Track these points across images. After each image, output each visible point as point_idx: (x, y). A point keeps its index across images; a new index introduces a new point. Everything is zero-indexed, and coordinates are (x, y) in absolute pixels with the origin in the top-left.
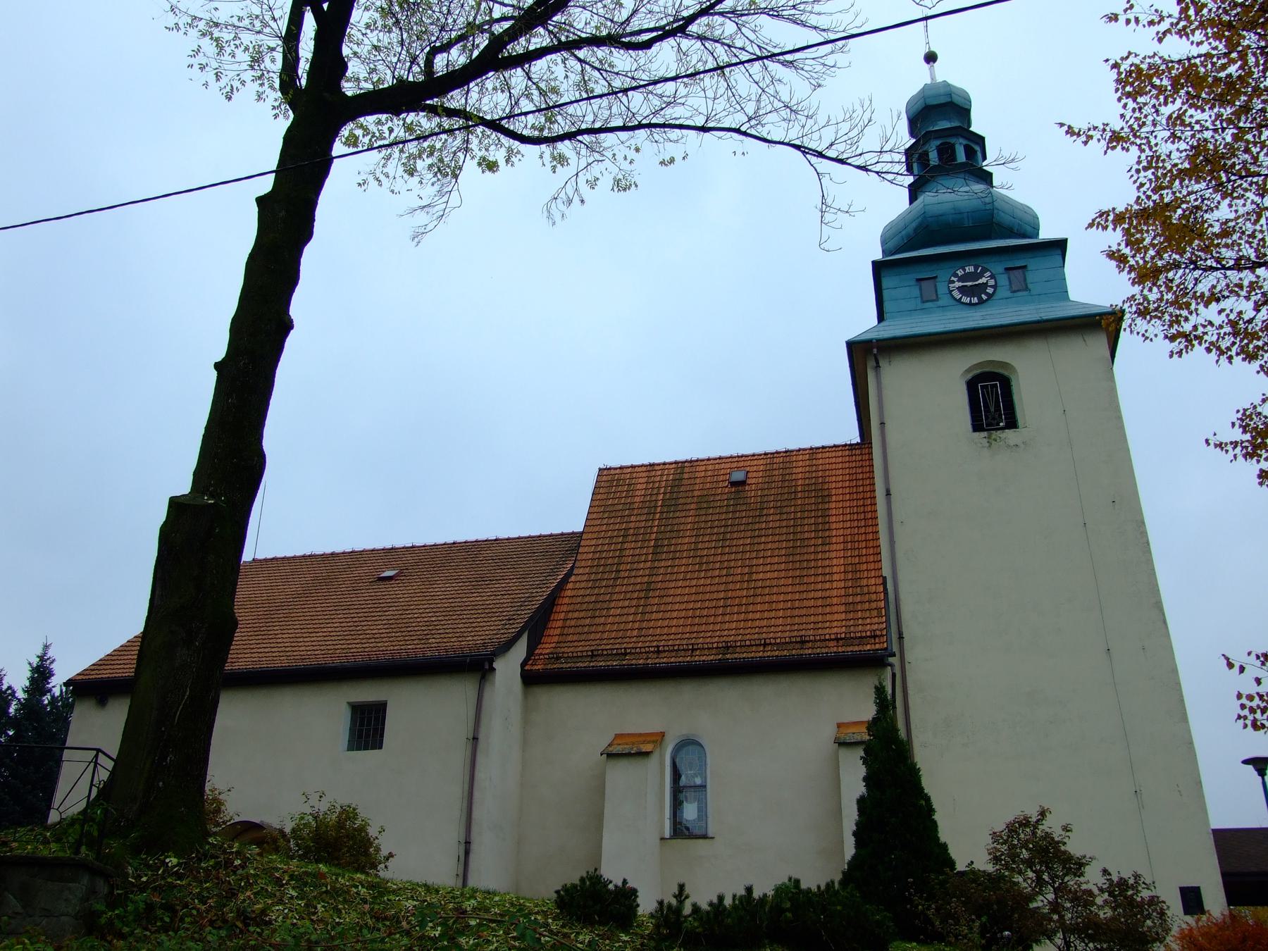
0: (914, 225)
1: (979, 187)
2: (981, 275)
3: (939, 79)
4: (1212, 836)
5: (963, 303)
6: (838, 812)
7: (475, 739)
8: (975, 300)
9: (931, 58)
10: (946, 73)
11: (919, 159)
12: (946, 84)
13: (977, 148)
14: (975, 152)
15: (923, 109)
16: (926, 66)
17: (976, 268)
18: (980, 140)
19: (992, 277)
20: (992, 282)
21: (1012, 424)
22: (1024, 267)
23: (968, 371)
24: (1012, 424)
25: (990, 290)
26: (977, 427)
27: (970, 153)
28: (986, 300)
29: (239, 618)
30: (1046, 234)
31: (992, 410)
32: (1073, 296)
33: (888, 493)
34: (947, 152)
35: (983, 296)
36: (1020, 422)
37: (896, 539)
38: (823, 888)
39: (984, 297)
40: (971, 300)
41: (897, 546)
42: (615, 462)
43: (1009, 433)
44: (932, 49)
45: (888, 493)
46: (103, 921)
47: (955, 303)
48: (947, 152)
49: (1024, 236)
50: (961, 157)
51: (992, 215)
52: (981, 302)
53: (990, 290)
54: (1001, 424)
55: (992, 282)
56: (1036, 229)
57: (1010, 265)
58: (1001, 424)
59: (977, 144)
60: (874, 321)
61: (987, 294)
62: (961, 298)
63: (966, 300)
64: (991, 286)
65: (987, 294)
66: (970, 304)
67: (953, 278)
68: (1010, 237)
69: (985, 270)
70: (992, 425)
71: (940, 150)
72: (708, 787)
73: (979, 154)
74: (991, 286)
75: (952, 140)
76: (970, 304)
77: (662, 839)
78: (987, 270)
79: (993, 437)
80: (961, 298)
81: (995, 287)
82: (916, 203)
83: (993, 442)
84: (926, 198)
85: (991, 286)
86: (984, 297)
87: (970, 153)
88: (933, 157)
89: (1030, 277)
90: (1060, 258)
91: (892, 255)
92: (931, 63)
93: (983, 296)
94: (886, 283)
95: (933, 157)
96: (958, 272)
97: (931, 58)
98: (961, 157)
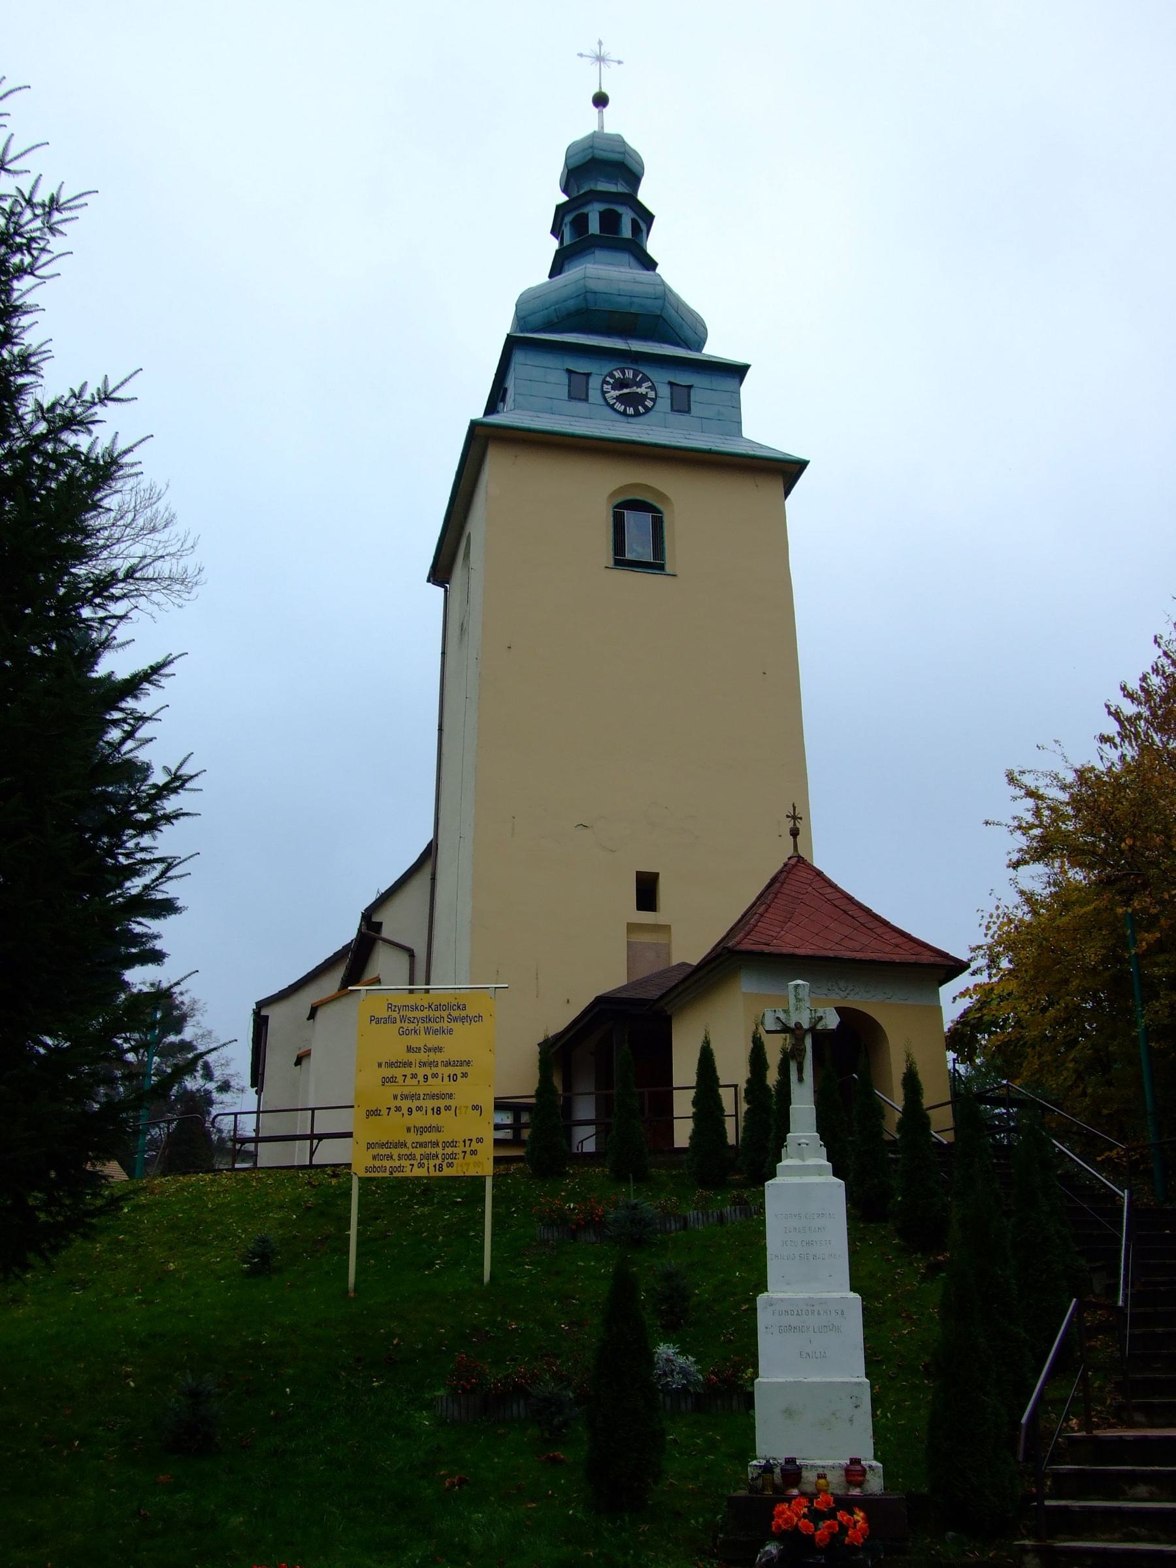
1: (644, 275)
2: (639, 385)
3: (609, 129)
5: (615, 410)
8: (631, 411)
9: (601, 100)
10: (615, 122)
11: (573, 223)
12: (619, 140)
13: (643, 227)
16: (596, 110)
17: (635, 376)
18: (649, 218)
19: (653, 388)
22: (690, 387)
23: (613, 495)
27: (636, 229)
28: (644, 414)
30: (715, 348)
32: (747, 432)
34: (610, 221)
35: (640, 407)
39: (641, 409)
40: (625, 409)
44: (604, 90)
46: (7, 264)
48: (610, 221)
49: (687, 345)
50: (627, 232)
52: (637, 414)
53: (649, 403)
55: (652, 394)
56: (699, 344)
60: (481, 416)
61: (645, 407)
63: (618, 406)
65: (645, 407)
66: (624, 414)
67: (608, 379)
68: (677, 345)
69: (646, 379)
71: (603, 216)
75: (620, 209)
78: (649, 380)
81: (654, 400)
82: (560, 279)
84: (574, 273)
85: (651, 399)
86: (641, 409)
87: (636, 229)
88: (594, 227)
91: (528, 332)
92: (601, 108)
93: (640, 407)
95: (594, 227)
97: (601, 100)
98: (627, 232)
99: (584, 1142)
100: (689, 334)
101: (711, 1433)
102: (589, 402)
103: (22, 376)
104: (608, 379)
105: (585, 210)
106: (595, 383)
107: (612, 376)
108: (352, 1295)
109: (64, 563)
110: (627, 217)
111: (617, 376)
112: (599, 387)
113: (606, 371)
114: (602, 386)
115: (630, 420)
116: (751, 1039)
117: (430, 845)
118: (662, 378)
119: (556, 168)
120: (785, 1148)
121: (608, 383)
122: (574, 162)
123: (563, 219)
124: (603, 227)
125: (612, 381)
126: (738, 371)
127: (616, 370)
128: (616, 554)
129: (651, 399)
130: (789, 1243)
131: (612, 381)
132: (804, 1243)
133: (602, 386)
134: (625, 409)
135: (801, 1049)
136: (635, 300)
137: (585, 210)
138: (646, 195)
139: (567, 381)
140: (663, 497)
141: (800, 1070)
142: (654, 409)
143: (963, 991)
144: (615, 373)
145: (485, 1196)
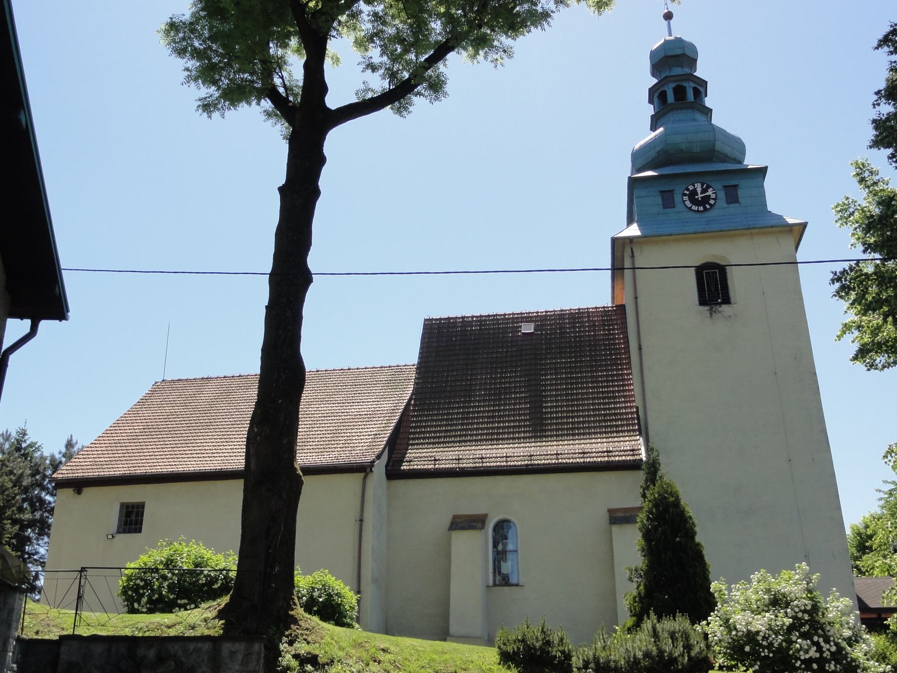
0: (658, 149)
3: (676, 34)
4: (483, 513)
5: (692, 210)
6: (487, 556)
7: (361, 520)
8: (701, 208)
9: (668, 16)
10: (682, 30)
12: (679, 40)
13: (701, 89)
14: (701, 92)
15: (664, 57)
16: (665, 23)
20: (713, 196)
21: (727, 301)
24: (727, 301)
25: (712, 202)
26: (702, 302)
29: (298, 458)
31: (713, 290)
32: (745, 163)
33: (640, 348)
34: (680, 92)
36: (732, 300)
37: (645, 381)
38: (645, 617)
39: (708, 206)
41: (646, 385)
42: (436, 315)
43: (725, 307)
45: (640, 348)
47: (687, 210)
48: (680, 92)
51: (714, 146)
52: (705, 209)
53: (712, 202)
54: (719, 301)
57: (726, 184)
58: (719, 301)
59: (702, 86)
61: (710, 204)
62: (691, 206)
63: (695, 208)
64: (712, 199)
65: (710, 204)
67: (686, 192)
70: (712, 301)
72: (519, 551)
73: (703, 94)
74: (712, 199)
75: (685, 84)
76: (698, 211)
77: (488, 586)
79: (714, 309)
80: (691, 206)
83: (713, 313)
85: (713, 199)
86: (708, 206)
88: (671, 98)
89: (741, 193)
90: (792, 243)
94: (636, 193)
95: (671, 98)
96: (689, 187)
100: (727, 150)
101: (285, 496)
104: (686, 192)
106: (677, 198)
107: (687, 189)
108: (152, 607)
109: (844, 662)
110: (689, 87)
113: (685, 187)
118: (718, 185)
119: (646, 65)
122: (657, 59)
124: (676, 99)
125: (688, 193)
126: (762, 172)
129: (713, 199)
131: (688, 193)
138: (700, 72)
143: (884, 454)
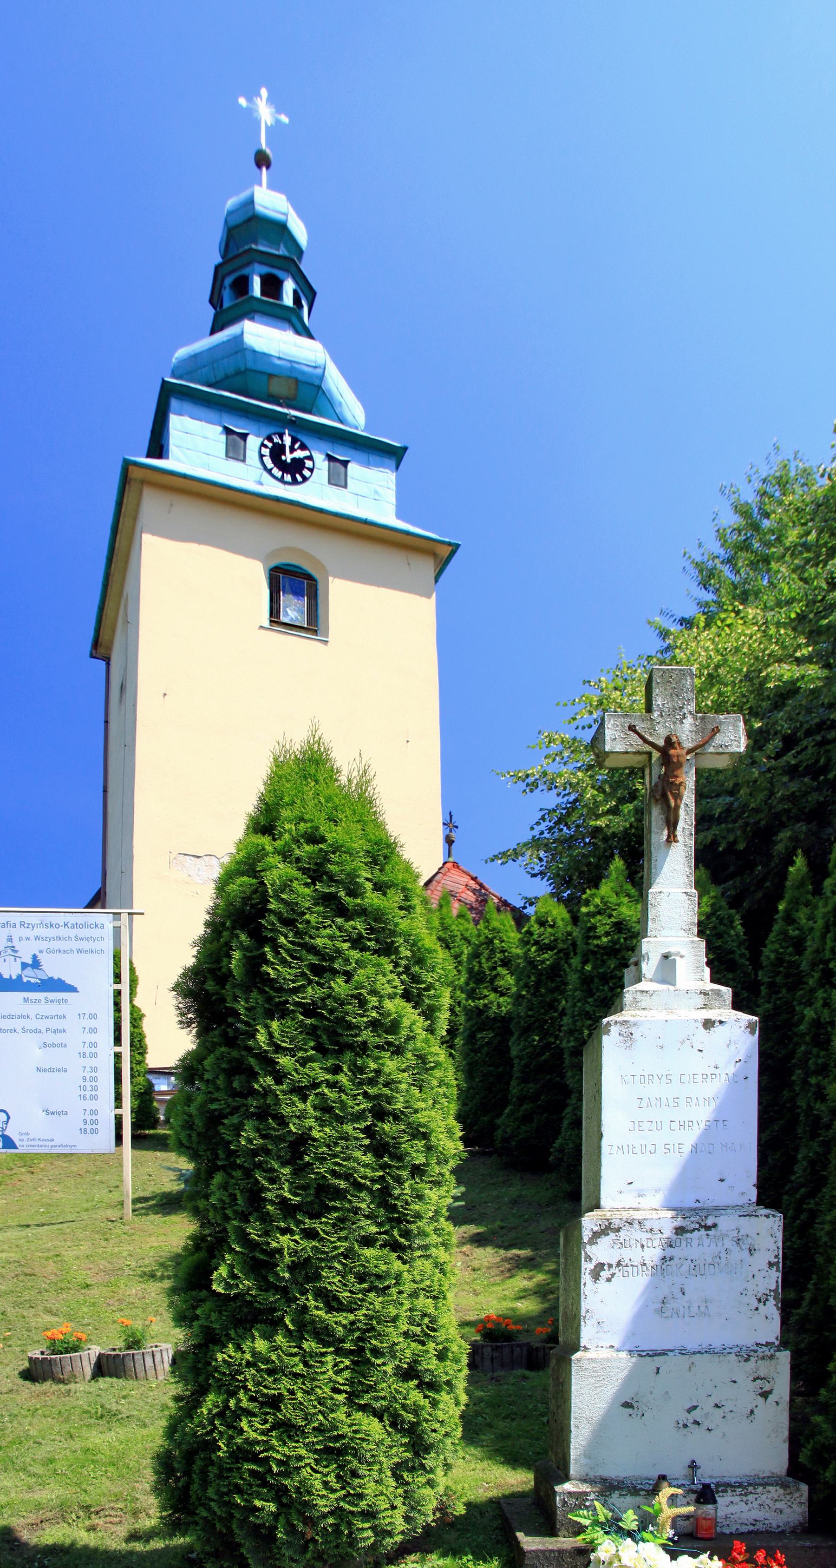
8: (288, 478)
67: (266, 442)
85: (309, 469)
99: (103, 664)
102: (247, 462)
103: (180, 1060)
104: (266, 442)
105: (245, 272)
111: (276, 440)
112: (257, 449)
114: (260, 449)
115: (287, 487)
116: (156, 1218)
117: (100, 890)
120: (632, 968)
121: (266, 447)
123: (223, 281)
125: (270, 445)
127: (275, 434)
128: (271, 615)
130: (646, 1126)
132: (675, 1126)
133: (260, 449)
134: (283, 476)
135: (677, 782)
136: (296, 366)
137: (245, 272)
139: (224, 440)
140: (318, 563)
141: (672, 824)
142: (311, 479)
144: (273, 437)
145: (132, 1130)
